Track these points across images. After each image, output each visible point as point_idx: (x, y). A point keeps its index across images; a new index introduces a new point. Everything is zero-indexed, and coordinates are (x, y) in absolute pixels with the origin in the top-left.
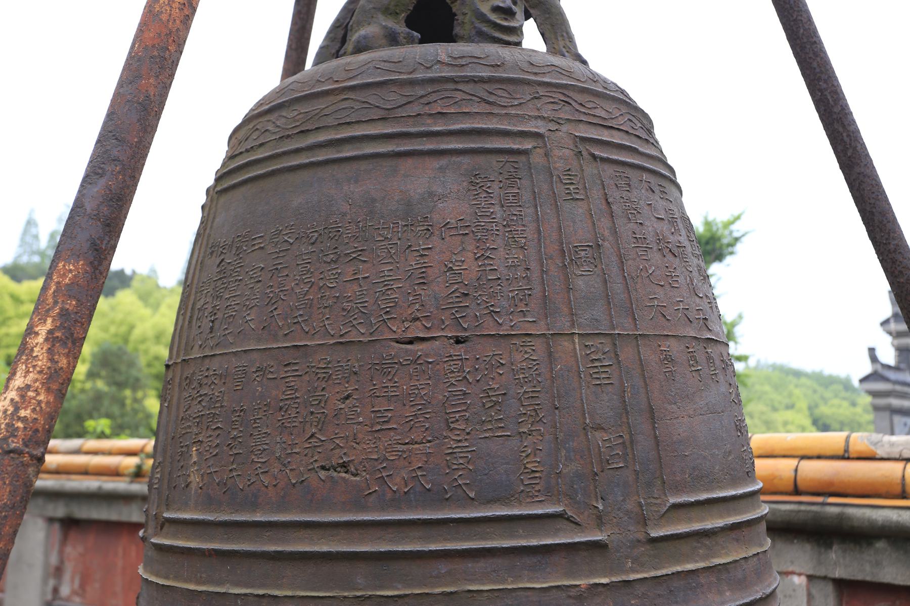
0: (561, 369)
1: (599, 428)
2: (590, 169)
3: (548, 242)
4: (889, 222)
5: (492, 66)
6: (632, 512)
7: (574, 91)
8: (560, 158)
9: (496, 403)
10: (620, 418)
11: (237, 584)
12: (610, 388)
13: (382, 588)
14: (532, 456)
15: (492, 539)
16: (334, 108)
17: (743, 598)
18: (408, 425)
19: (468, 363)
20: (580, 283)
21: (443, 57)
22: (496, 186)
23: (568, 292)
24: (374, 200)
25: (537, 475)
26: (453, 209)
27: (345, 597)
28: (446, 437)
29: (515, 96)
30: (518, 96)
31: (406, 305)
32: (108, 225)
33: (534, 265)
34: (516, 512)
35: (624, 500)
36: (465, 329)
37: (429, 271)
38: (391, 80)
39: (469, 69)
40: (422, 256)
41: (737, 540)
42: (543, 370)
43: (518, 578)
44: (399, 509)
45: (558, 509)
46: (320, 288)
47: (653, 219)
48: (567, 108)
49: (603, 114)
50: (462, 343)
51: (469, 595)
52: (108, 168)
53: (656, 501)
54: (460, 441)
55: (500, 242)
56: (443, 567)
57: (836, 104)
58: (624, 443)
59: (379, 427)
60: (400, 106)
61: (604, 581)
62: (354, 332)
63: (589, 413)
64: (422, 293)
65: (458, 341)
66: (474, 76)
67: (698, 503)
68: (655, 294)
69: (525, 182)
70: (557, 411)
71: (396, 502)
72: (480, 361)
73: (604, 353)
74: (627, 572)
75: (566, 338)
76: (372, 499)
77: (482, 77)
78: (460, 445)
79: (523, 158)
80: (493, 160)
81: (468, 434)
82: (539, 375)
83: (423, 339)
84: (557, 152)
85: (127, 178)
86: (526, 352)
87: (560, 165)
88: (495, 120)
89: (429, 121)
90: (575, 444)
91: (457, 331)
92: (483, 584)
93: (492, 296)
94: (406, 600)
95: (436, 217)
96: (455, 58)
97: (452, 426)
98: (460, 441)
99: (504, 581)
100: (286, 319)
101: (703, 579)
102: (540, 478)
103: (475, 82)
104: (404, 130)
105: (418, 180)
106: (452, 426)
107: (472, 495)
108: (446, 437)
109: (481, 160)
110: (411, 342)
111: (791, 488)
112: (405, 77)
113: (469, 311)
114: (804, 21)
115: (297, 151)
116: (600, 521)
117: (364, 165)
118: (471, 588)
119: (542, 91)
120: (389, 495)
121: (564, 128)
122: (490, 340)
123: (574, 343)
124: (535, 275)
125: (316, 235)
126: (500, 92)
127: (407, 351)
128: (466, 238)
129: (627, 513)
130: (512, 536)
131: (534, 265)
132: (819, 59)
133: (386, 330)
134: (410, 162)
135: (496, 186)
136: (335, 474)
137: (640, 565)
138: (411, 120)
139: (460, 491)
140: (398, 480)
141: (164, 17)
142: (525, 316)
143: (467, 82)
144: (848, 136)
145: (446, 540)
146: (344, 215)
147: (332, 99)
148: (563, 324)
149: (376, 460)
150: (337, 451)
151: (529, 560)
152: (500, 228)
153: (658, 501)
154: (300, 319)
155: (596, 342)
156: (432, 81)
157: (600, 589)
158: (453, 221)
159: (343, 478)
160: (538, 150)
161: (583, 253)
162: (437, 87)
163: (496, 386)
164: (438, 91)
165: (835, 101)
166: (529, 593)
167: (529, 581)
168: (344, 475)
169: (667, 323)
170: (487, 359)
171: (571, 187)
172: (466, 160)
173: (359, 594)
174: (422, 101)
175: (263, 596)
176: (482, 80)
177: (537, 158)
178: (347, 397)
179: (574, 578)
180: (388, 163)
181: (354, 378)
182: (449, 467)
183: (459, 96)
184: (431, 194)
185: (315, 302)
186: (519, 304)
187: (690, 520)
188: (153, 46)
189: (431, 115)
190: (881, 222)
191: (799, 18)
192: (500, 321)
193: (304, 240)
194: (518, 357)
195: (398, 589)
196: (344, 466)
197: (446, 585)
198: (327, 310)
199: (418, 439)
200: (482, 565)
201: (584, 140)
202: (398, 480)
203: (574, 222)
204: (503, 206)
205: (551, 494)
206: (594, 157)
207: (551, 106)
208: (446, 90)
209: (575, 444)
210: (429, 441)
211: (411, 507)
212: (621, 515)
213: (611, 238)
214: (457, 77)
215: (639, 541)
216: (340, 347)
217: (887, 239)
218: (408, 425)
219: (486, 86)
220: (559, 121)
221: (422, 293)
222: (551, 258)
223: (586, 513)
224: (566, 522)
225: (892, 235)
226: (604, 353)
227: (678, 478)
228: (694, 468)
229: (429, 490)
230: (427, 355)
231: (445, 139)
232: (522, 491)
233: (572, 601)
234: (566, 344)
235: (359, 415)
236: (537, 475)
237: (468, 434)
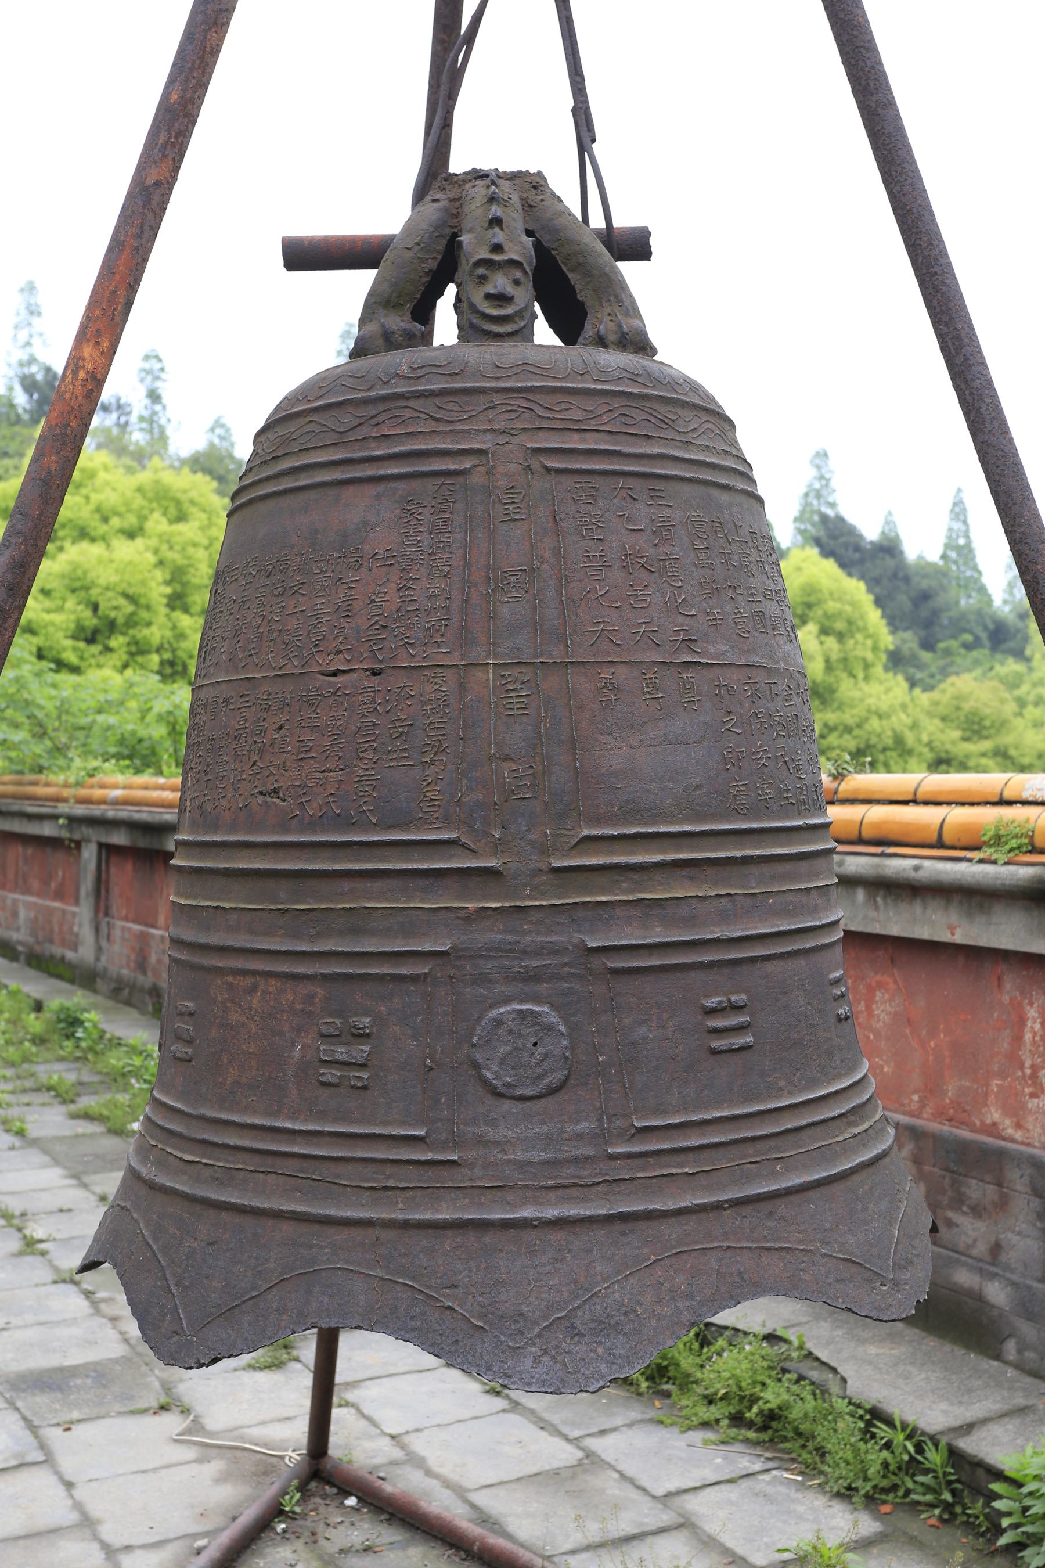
0: (471, 700)
1: (507, 758)
2: (541, 484)
3: (474, 569)
4: (1015, 504)
5: (450, 375)
6: (536, 842)
7: (541, 393)
8: (504, 474)
9: (402, 733)
10: (534, 749)
11: (205, 899)
12: (524, 719)
13: (297, 902)
14: (433, 784)
15: (390, 861)
16: (300, 432)
17: (680, 935)
18: (325, 755)
19: (380, 694)
20: (505, 611)
21: (405, 370)
22: (427, 512)
23: (489, 621)
24: (316, 532)
25: (436, 803)
26: (382, 540)
27: (271, 910)
28: (355, 766)
29: (466, 408)
30: (470, 408)
31: (331, 638)
32: (11, 589)
33: (456, 594)
34: (412, 837)
35: (528, 830)
36: (381, 662)
37: (355, 603)
38: (348, 400)
39: (424, 381)
40: (350, 588)
41: (691, 878)
42: (452, 701)
43: (410, 898)
44: (314, 832)
45: (453, 835)
46: (269, 621)
47: (623, 531)
48: (527, 415)
49: (577, 415)
50: (379, 674)
51: (366, 911)
52: (13, 540)
53: (567, 833)
54: (367, 770)
55: (423, 570)
56: (346, 885)
57: (958, 354)
58: (533, 774)
59: (302, 756)
60: (351, 429)
61: (494, 905)
62: (289, 665)
63: (496, 744)
64: (346, 625)
65: (375, 673)
66: (424, 390)
67: (614, 838)
68: (603, 617)
69: (460, 506)
70: (461, 742)
71: (313, 825)
72: (392, 692)
73: (523, 683)
74: (524, 899)
75: (480, 668)
76: (295, 821)
77: (433, 391)
78: (368, 773)
79: (461, 479)
80: (430, 484)
81: (375, 763)
82: (448, 705)
83: (344, 672)
84: (501, 469)
85: (29, 548)
86: (436, 683)
87: (502, 483)
88: (437, 439)
89: (373, 445)
90: (478, 774)
91: (373, 663)
92: (380, 902)
93: (409, 627)
94: (315, 913)
95: (367, 548)
96: (415, 369)
97: (361, 755)
98: (367, 770)
99: (397, 900)
100: (244, 651)
101: (619, 912)
102: (439, 806)
103: (426, 396)
104: (349, 456)
105: (357, 508)
106: (361, 755)
107: (374, 820)
108: (355, 766)
109: (417, 484)
110: (335, 674)
111: (934, 837)
112: (360, 396)
113: (386, 642)
114: (924, 245)
115: (268, 479)
116: (497, 847)
117: (313, 495)
118: (368, 905)
119: (498, 399)
120: (307, 819)
121: (516, 440)
122: (403, 672)
123: (488, 673)
124: (456, 605)
125: (271, 567)
126: (450, 406)
127: (329, 682)
128: (392, 568)
129: (531, 843)
130: (408, 860)
131: (456, 594)
132: (939, 295)
133: (314, 662)
134: (351, 490)
135: (427, 512)
136: (269, 799)
137: (538, 891)
138: (357, 445)
139: (364, 816)
140: (315, 805)
141: (67, 396)
142: (439, 647)
143: (418, 397)
144: (971, 394)
145: (350, 861)
146: (293, 546)
147: (302, 421)
148: (479, 653)
149: (299, 786)
150: (271, 778)
151: (421, 882)
152: (425, 556)
153: (571, 833)
154: (253, 652)
155: (515, 672)
156: (384, 399)
157: (489, 912)
158: (381, 551)
159: (274, 803)
160: (480, 469)
161: (513, 579)
162: (388, 405)
163: (403, 717)
164: (388, 410)
165: (956, 349)
166: (419, 912)
167: (421, 902)
168: (275, 800)
169: (615, 648)
170: (398, 691)
171: (511, 507)
172: (401, 486)
173: (280, 907)
174: (373, 422)
175: (216, 908)
176: (432, 394)
177: (477, 478)
178: (281, 728)
179: (466, 901)
180: (332, 492)
181: (287, 709)
182: (356, 794)
183: (407, 413)
184: (365, 524)
185: (264, 635)
186: (435, 635)
187: (613, 853)
188: (56, 425)
189: (375, 438)
190: (1006, 505)
191: (918, 242)
192: (413, 653)
193: (263, 572)
194: (428, 688)
195: (310, 904)
196: (275, 791)
197: (348, 902)
198: (272, 644)
199: (332, 768)
200: (378, 885)
201: (536, 451)
202: (315, 805)
203: (509, 545)
204: (431, 533)
205: (448, 821)
206: (548, 470)
207: (507, 416)
208: (396, 408)
209: (478, 774)
210: (342, 770)
211: (324, 831)
212: (523, 844)
213: (552, 560)
214: (408, 392)
215: (541, 870)
216: (279, 679)
217: (1012, 526)
218: (325, 755)
219: (437, 401)
220: (512, 432)
221: (346, 625)
222: (475, 586)
223: (484, 841)
224: (461, 849)
225: (1018, 520)
226: (523, 683)
227: (601, 811)
228: (627, 802)
229: (338, 815)
230: (345, 687)
231: (387, 463)
232: (421, 818)
233: (460, 922)
234: (480, 674)
235: (288, 744)
236: (436, 803)
237: (375, 763)
